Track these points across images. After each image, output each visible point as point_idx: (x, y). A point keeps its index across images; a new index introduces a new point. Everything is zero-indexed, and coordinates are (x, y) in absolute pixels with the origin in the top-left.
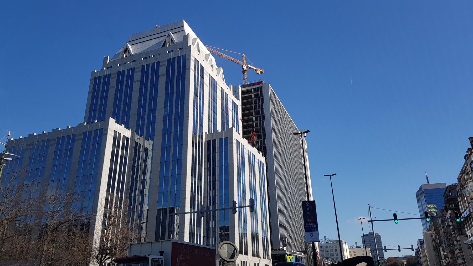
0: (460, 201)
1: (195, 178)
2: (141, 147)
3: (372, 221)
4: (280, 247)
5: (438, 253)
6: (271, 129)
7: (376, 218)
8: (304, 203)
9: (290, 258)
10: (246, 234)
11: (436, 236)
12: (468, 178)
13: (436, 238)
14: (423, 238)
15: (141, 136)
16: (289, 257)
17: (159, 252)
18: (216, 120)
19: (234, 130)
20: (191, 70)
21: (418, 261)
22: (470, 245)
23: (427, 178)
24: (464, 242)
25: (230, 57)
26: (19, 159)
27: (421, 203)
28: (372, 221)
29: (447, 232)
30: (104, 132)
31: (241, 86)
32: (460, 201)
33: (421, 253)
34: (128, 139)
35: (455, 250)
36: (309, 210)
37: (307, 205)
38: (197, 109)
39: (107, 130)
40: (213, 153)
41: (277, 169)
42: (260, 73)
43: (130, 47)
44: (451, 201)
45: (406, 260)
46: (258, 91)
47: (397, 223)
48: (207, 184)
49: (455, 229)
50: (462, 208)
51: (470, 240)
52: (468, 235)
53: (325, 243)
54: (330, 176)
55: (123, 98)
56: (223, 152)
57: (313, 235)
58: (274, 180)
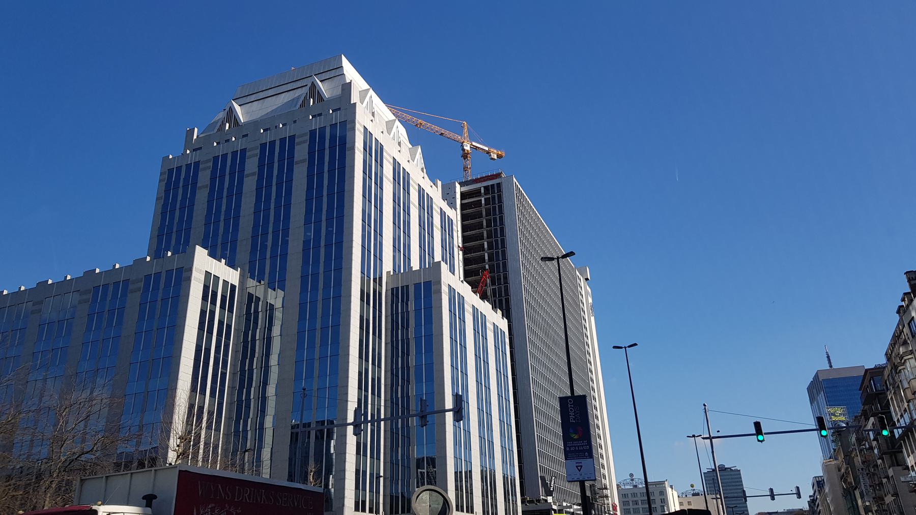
0: (892, 398)
2: (260, 303)
3: (711, 438)
4: (541, 497)
5: (853, 504)
6: (518, 265)
7: (718, 431)
8: (563, 401)
10: (471, 472)
11: (847, 469)
12: (906, 352)
13: (847, 473)
14: (822, 475)
15: (260, 282)
17: (144, 498)
18: (408, 247)
19: (444, 268)
20: (356, 151)
22: (913, 486)
23: (828, 357)
24: (903, 479)
25: (437, 128)
26: (19, 331)
27: (819, 406)
28: (711, 438)
29: (869, 461)
30: (185, 275)
31: (459, 183)
32: (892, 398)
34: (233, 287)
35: (886, 496)
36: (571, 415)
37: (570, 405)
38: (370, 226)
39: (190, 270)
40: (402, 313)
41: (531, 342)
42: (496, 158)
46: (493, 192)
47: (761, 441)
48: (392, 373)
49: (885, 454)
50: (897, 412)
51: (913, 475)
52: (910, 466)
53: (632, 487)
54: (625, 348)
55: (224, 208)
56: (423, 310)
57: (581, 466)
58: (527, 364)
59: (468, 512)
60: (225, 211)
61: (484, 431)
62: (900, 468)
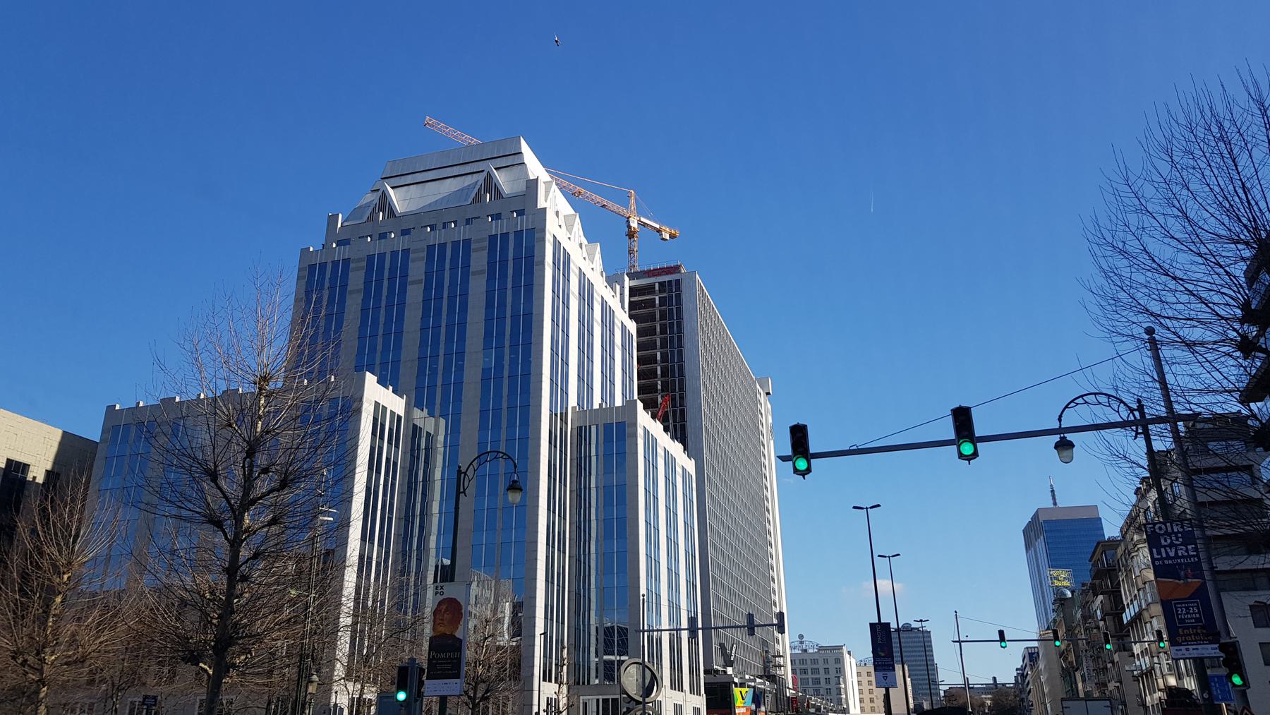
0: (1123, 580)
1: (381, 441)
3: (960, 642)
4: (715, 667)
5: (1072, 687)
6: (698, 385)
8: (872, 625)
9: (741, 692)
16: (740, 689)
21: (1022, 700)
23: (1053, 491)
24: (1127, 668)
25: (599, 198)
28: (960, 642)
32: (1123, 580)
33: (1031, 682)
34: (399, 418)
35: (1109, 682)
39: (361, 400)
42: (668, 238)
43: (391, 191)
44: (1106, 574)
45: (990, 696)
52: (1136, 654)
59: (679, 690)
60: (384, 324)
61: (672, 593)
62: (1126, 653)
